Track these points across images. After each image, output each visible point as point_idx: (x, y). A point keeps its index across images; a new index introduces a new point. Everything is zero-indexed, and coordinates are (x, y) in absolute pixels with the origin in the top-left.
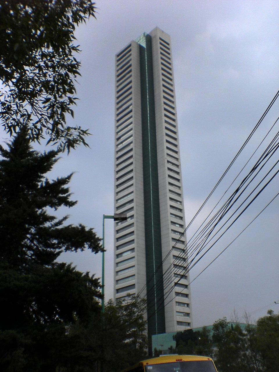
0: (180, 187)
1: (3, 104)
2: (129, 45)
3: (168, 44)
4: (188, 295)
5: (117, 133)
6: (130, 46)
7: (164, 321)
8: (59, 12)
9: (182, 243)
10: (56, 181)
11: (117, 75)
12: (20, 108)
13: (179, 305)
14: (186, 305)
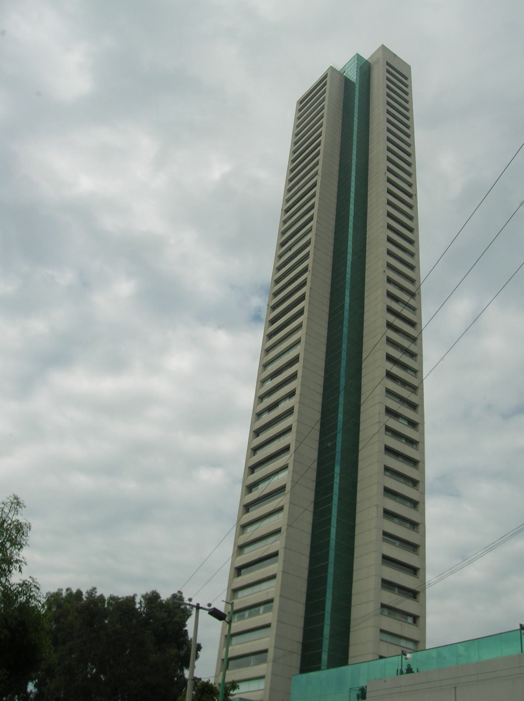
0: (416, 309)
1: (1, 508)
2: (278, 529)
3: (406, 78)
4: (419, 617)
5: (244, 527)
6: (325, 77)
7: (369, 112)
8: (53, 629)
9: (411, 484)
10: (98, 594)
11: (278, 254)
12: (22, 540)
13: (389, 615)
14: (410, 620)
